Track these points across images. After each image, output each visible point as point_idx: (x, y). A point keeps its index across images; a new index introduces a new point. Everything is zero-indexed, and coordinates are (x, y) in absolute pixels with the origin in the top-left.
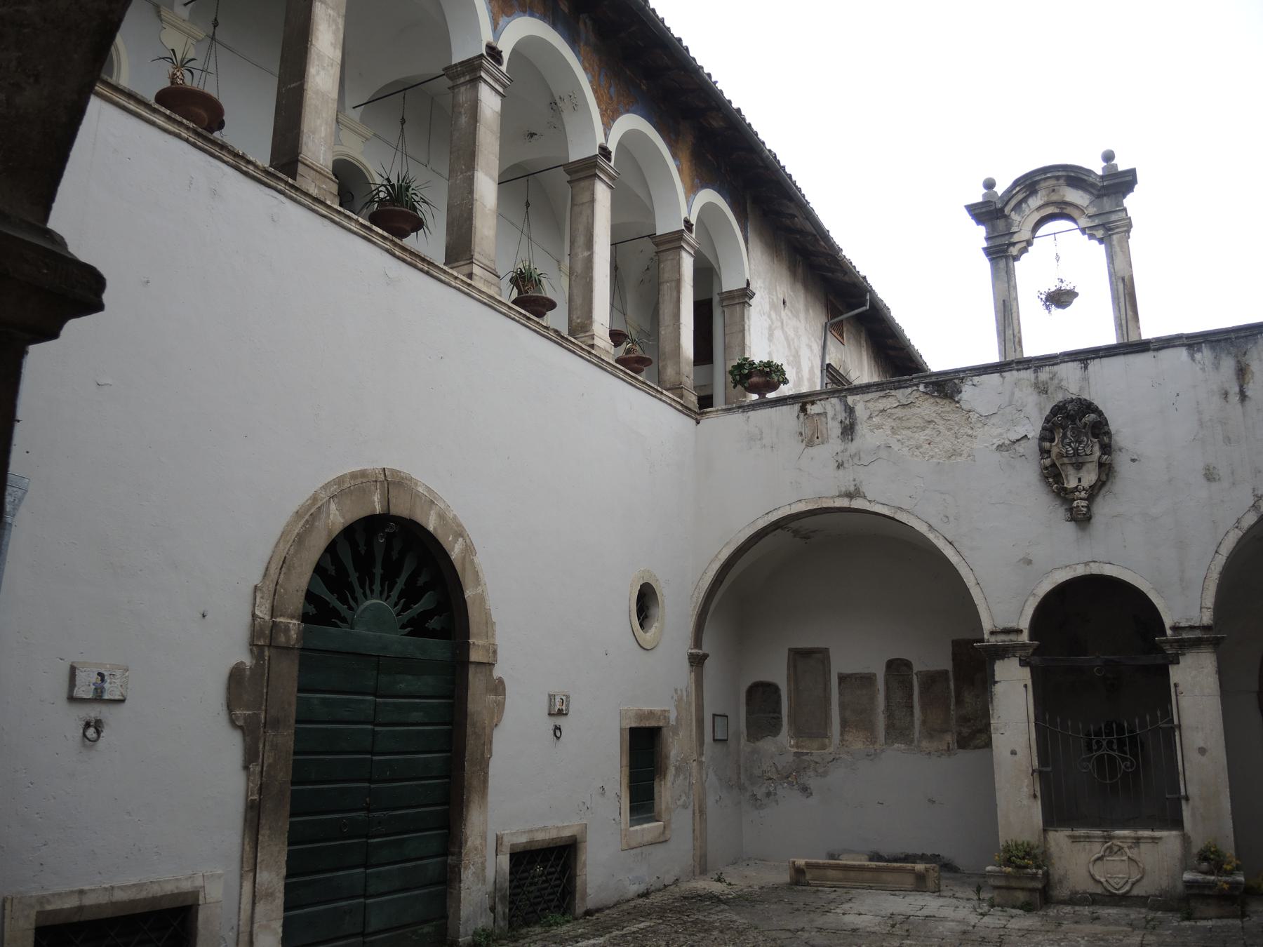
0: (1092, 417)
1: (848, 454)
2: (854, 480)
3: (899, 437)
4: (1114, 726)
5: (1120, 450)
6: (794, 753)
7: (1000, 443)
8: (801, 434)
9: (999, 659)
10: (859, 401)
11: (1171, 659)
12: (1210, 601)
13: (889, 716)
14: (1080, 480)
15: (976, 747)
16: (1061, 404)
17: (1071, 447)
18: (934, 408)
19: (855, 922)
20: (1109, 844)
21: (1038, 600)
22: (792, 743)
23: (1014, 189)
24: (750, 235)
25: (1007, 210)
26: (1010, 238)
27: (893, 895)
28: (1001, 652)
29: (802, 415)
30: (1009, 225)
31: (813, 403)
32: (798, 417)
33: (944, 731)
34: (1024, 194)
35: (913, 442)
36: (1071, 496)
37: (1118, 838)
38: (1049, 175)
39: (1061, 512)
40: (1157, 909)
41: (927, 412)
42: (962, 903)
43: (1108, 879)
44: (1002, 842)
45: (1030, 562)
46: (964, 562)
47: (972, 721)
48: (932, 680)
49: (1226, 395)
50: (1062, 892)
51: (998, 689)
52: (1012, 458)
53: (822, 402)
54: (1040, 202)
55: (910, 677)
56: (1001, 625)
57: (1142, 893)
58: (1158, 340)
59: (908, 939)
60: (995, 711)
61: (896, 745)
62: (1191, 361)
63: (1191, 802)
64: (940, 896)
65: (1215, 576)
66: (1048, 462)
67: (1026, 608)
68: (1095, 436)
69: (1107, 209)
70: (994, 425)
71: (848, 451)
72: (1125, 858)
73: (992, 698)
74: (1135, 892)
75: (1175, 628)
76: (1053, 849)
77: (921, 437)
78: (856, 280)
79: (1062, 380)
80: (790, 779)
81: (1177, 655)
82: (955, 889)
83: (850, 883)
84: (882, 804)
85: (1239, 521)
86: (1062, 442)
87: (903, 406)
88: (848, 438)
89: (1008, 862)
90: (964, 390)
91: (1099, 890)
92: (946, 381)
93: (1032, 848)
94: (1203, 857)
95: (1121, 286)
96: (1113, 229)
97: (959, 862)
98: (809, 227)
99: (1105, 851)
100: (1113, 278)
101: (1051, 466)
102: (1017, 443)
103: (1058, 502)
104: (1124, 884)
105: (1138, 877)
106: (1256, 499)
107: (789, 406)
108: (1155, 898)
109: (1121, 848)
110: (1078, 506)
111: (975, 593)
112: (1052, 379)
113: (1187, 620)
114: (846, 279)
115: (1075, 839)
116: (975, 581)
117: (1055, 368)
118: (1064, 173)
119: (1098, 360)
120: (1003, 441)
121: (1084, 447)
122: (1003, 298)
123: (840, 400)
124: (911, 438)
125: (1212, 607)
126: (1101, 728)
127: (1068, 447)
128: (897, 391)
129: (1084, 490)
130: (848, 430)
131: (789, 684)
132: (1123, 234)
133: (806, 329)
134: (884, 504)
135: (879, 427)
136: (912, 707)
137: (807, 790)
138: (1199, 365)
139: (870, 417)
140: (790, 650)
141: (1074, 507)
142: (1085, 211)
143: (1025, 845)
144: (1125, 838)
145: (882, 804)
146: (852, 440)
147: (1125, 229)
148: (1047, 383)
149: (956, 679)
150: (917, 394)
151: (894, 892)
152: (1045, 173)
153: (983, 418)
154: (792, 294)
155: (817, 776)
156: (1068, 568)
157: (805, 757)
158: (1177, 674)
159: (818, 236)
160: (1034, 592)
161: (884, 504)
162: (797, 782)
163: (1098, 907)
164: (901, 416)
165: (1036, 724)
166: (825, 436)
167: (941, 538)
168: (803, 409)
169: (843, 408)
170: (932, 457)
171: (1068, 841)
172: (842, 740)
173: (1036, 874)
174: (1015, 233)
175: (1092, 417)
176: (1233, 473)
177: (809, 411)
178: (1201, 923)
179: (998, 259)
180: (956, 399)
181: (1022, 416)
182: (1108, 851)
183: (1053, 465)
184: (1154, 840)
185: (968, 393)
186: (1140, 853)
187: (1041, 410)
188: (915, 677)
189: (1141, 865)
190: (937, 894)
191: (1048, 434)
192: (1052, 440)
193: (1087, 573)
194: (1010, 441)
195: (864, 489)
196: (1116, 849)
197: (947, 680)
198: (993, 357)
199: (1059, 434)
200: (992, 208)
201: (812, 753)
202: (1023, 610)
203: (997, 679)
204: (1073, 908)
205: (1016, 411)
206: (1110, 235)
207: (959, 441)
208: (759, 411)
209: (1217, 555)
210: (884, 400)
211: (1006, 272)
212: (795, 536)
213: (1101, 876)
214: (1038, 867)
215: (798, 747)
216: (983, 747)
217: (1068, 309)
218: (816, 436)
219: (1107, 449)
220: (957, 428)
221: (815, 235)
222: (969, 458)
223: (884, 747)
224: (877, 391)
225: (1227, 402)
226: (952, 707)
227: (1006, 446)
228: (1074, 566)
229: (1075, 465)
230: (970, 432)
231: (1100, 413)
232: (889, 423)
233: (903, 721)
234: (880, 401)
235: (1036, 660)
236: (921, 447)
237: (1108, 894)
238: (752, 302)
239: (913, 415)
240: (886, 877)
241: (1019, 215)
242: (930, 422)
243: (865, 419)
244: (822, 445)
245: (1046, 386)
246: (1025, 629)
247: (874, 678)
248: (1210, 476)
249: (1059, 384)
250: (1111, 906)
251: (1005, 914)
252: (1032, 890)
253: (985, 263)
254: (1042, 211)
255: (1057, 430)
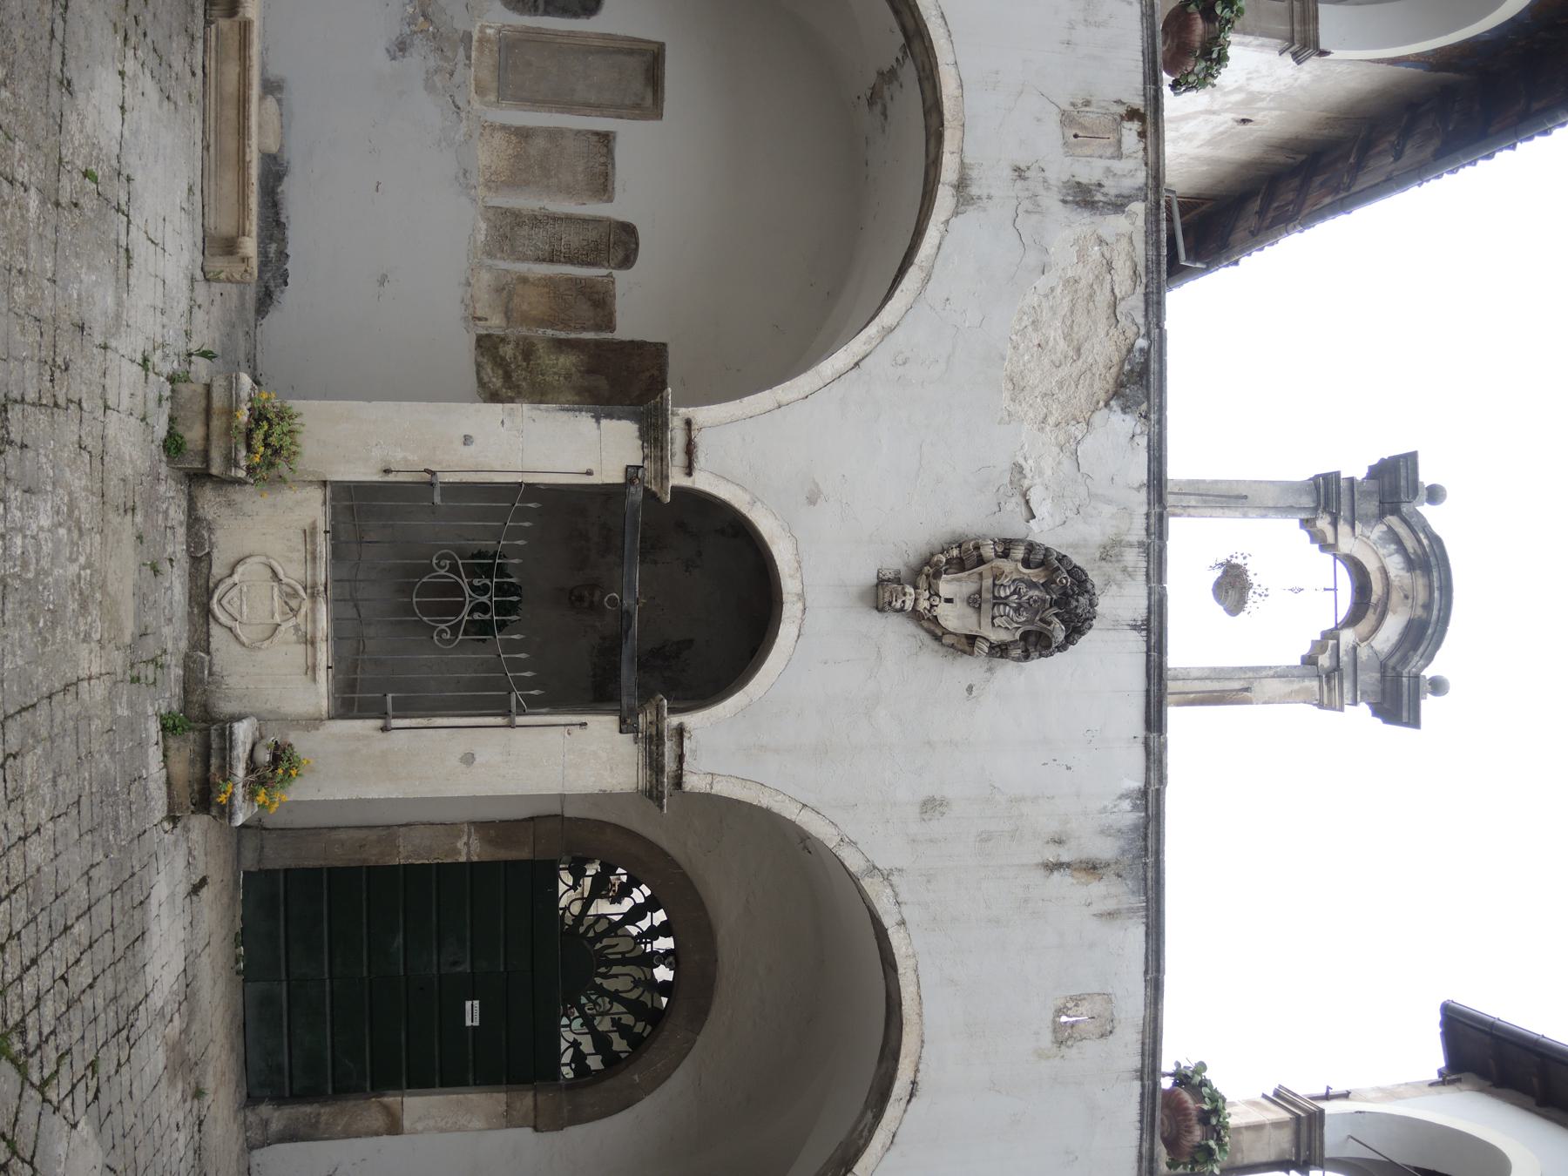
0: (1059, 631)
1: (1041, 191)
2: (989, 197)
3: (1059, 290)
4: (515, 599)
5: (990, 670)
6: (470, 33)
7: (1027, 471)
8: (1087, 103)
9: (640, 430)
10: (1134, 224)
11: (629, 721)
12: (723, 788)
13: (536, 217)
14: (949, 601)
15: (479, 366)
16: (1090, 587)
17: (1012, 594)
18: (1101, 360)
19: (95, 94)
20: (302, 593)
21: (744, 509)
22: (489, 31)
23: (1427, 537)
24: (1401, 69)
25: (1393, 520)
26: (1345, 520)
27: (190, 189)
28: (653, 433)
29: (1122, 110)
30: (1366, 521)
31: (1142, 135)
32: (1119, 102)
33: (507, 314)
34: (1410, 550)
35: (1046, 315)
36: (922, 582)
37: (314, 610)
38: (1436, 594)
39: (895, 562)
40: (186, 667)
41: (1098, 348)
42: (177, 324)
43: (238, 587)
44: (296, 405)
45: (812, 500)
46: (822, 385)
47: (525, 364)
48: (600, 302)
49: (1059, 842)
50: (210, 502)
51: (585, 422)
52: (998, 490)
53: (1141, 153)
54: (1392, 573)
55: (607, 265)
56: (701, 439)
57: (214, 643)
58: (1163, 747)
59: (43, 202)
60: (545, 414)
61: (483, 226)
62: (1119, 792)
63: (380, 734)
64: (193, 280)
65: (764, 800)
66: (988, 551)
67: (733, 488)
68: (1025, 636)
69: (1361, 677)
70: (1059, 463)
71: (1045, 193)
72: (278, 619)
73: (568, 410)
74: (215, 630)
75: (680, 731)
76: (289, 496)
77: (1054, 333)
78: (1235, 249)
79: (1120, 586)
80: (421, 19)
81: (636, 730)
82: (215, 310)
83: (213, 106)
84: (377, 190)
85: (853, 843)
86: (1021, 580)
87: (1114, 306)
88: (1068, 194)
89: (258, 416)
90: (1128, 418)
91: (218, 570)
92: (1148, 388)
93: (288, 460)
94: (280, 754)
95: (1236, 685)
96: (1328, 682)
97: (273, 318)
98: (1364, 181)
99: (288, 585)
100: (1250, 674)
101: (980, 555)
102: (1023, 501)
103: (913, 560)
104: (230, 615)
105: (244, 639)
106: (885, 872)
107: (1141, 87)
108: (207, 664)
109: (295, 612)
110: (905, 595)
111: (765, 399)
112: (1124, 570)
113: (694, 752)
114: (1239, 234)
115: (309, 534)
116: (785, 403)
117: (1141, 578)
118: (1434, 617)
119: (1144, 649)
120: (1029, 475)
121: (1008, 616)
122: (1249, 496)
123: (1140, 189)
124: (1055, 314)
125: (713, 792)
126: (511, 577)
127: (1012, 589)
128: (1142, 298)
129: (932, 606)
130: (1083, 197)
131: (605, 36)
132: (1318, 697)
133: (1181, 155)
134: (939, 248)
135: (1082, 256)
136: (552, 260)
137: (400, 50)
138: (1111, 806)
139: (1101, 241)
140: (662, 46)
141: (903, 588)
142: (1365, 643)
143: (293, 448)
144: (314, 621)
145: (377, 190)
146: (1064, 202)
147: (1326, 701)
148: (1118, 561)
149: (598, 344)
150: (1130, 334)
151: (198, 193)
152: (1440, 589)
153: (1074, 447)
154: (1252, 138)
155: (427, 72)
156: (796, 565)
157: (461, 52)
158: (603, 726)
159: (1343, 194)
160: (759, 504)
161: (939, 248)
162: (415, 32)
163: (187, 566)
164: (1097, 299)
165: (520, 484)
166: (1078, 151)
167: (867, 348)
168: (1133, 114)
169: (1126, 192)
170: (1015, 348)
171: (306, 523)
172: (493, 127)
173: (237, 466)
174: (1353, 528)
175: (1059, 631)
176: (931, 841)
177: (1127, 125)
178: (154, 755)
179: (1315, 495)
180: (1113, 403)
181: (1068, 513)
182: (289, 590)
183: (981, 561)
184: (312, 669)
185: (1121, 424)
186: (287, 643)
187: (1075, 546)
188: (603, 272)
189: (266, 644)
190: (199, 275)
191: (1039, 558)
192: (1026, 563)
193: (784, 596)
194: (1028, 489)
195: (971, 215)
196: (294, 603)
197: (598, 328)
198: (1176, 470)
199: (1036, 576)
200: (1403, 497)
201: (469, 66)
202: (728, 480)
203: (604, 422)
204: (181, 524)
205: (1078, 503)
206: (1319, 677)
207: (1038, 400)
208: (1140, 27)
209: (800, 806)
210: (1128, 272)
211: (1292, 507)
212: (881, 74)
213: (243, 574)
214: (250, 470)
215: (480, 41)
216: (482, 383)
217: (1211, 593)
218: (1080, 134)
219: (1000, 650)
220: (1061, 399)
221: (1349, 188)
222: (1006, 413)
223: (480, 202)
224: (1147, 260)
225: (1048, 842)
226: (550, 332)
227: (1019, 480)
228: (798, 575)
229: (977, 596)
230: (1051, 420)
231: (1062, 648)
232: (1087, 277)
233: (527, 242)
234: (1128, 263)
235: (636, 494)
236: (1036, 330)
237: (211, 585)
238: (1288, 58)
239: (1095, 322)
240: (230, 178)
241: (1380, 538)
242: (1078, 350)
243: (1100, 232)
244: (1061, 142)
245: (1113, 559)
246: (694, 482)
247: (605, 197)
248: (929, 807)
249: (1114, 581)
250: (190, 590)
251: (152, 404)
252: (206, 455)
253: (1303, 471)
254: (1379, 576)
255: (1043, 574)
